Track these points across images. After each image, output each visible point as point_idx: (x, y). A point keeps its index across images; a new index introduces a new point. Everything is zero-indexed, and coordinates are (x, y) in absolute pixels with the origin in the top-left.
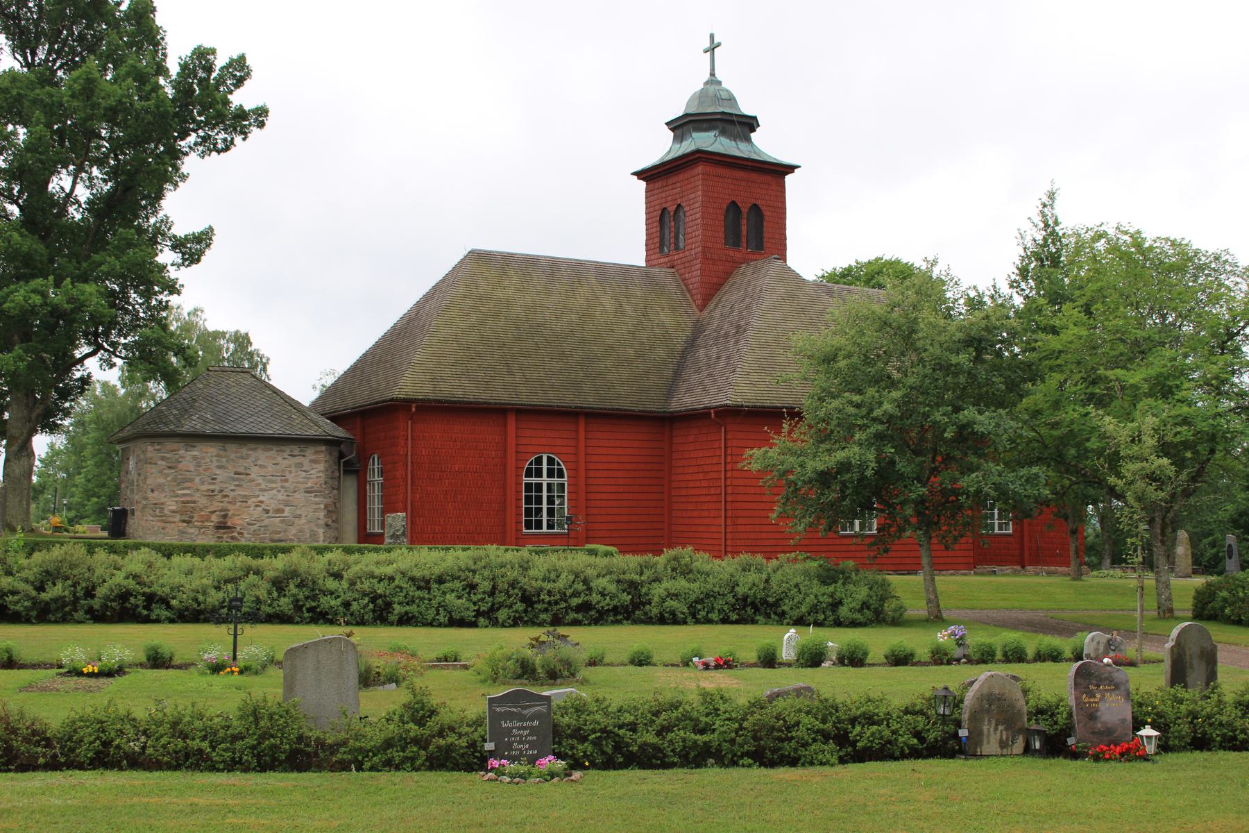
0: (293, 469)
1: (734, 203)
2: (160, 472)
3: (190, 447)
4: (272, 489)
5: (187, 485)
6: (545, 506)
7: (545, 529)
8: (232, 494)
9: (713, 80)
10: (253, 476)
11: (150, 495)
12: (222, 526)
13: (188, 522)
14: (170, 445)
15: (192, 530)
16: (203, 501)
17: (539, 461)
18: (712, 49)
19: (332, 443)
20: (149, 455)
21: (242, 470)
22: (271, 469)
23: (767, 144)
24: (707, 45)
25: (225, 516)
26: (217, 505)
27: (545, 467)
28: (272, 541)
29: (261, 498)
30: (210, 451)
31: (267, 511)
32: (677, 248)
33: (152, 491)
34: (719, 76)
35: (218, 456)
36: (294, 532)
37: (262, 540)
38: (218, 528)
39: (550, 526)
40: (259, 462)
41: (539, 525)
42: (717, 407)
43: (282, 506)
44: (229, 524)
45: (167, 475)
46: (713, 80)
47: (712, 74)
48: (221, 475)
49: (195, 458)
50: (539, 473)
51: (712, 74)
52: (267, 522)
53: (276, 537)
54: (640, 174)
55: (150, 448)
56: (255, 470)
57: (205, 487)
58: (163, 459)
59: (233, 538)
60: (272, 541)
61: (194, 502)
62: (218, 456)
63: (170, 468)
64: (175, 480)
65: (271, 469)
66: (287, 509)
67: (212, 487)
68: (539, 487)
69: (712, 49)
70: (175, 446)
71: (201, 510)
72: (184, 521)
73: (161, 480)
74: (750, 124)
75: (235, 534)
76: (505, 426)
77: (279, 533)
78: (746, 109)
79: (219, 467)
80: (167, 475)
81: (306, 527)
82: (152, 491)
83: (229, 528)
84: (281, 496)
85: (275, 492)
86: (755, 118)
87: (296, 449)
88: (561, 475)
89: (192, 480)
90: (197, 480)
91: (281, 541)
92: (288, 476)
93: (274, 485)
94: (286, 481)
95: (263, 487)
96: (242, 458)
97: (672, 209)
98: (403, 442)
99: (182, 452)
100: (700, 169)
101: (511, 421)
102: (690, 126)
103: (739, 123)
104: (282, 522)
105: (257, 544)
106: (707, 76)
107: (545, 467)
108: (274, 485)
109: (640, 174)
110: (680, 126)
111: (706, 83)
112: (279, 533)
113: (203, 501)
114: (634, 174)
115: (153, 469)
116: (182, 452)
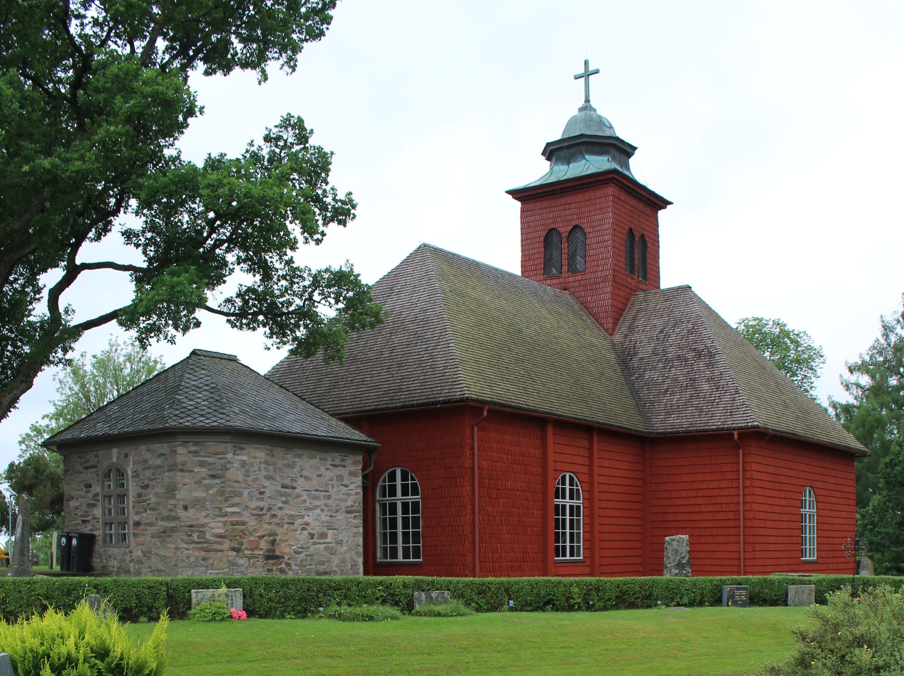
0: (335, 483)
1: (631, 229)
2: (199, 483)
3: (238, 449)
4: (316, 507)
5: (236, 500)
6: (400, 530)
7: (400, 558)
8: (280, 514)
9: (587, 107)
10: (299, 490)
11: (181, 513)
12: (271, 556)
13: (237, 550)
14: (212, 445)
15: (242, 561)
16: (252, 523)
17: (392, 477)
18: (587, 75)
19: (367, 451)
20: (179, 459)
21: (288, 482)
22: (315, 482)
23: (640, 170)
24: (582, 71)
25: (273, 542)
26: (265, 528)
27: (399, 482)
28: (318, 573)
29: (306, 519)
30: (256, 454)
31: (312, 536)
32: (573, 270)
33: (186, 508)
34: (593, 103)
35: (266, 462)
36: (336, 562)
37: (308, 572)
38: (268, 557)
39: (406, 556)
40: (305, 473)
41: (394, 554)
42: (742, 428)
43: (325, 530)
44: (277, 553)
45: (208, 487)
46: (587, 107)
47: (587, 100)
48: (271, 488)
49: (243, 464)
50: (393, 493)
51: (587, 100)
52: (312, 549)
53: (322, 568)
54: (516, 194)
55: (181, 450)
56: (301, 481)
57: (254, 504)
58: (202, 464)
59: (282, 571)
60: (318, 573)
61: (243, 524)
62: (266, 462)
63: (213, 477)
64: (221, 492)
65: (315, 482)
66: (330, 532)
67: (261, 504)
68: (405, 493)
69: (587, 75)
70: (221, 447)
71: (251, 534)
72: (233, 549)
73: (200, 494)
74: (625, 150)
75: (283, 566)
76: (544, 439)
77: (323, 563)
78: (623, 133)
79: (268, 478)
80: (208, 487)
81: (348, 556)
82: (186, 508)
83: (277, 557)
84: (325, 518)
85: (318, 511)
86: (635, 149)
87: (337, 458)
88: (415, 492)
89: (240, 495)
90: (246, 493)
91: (325, 573)
92: (332, 492)
93: (317, 503)
94: (329, 497)
95: (308, 504)
96: (288, 466)
97: (564, 230)
98: (468, 452)
99: (230, 456)
100: (611, 190)
101: (550, 430)
102: (583, 148)
103: (568, 147)
104: (326, 549)
105: (303, 576)
106: (581, 103)
107: (399, 482)
108: (317, 503)
109: (516, 194)
110: (552, 152)
111: (581, 110)
112: (323, 563)
113: (252, 523)
114: (509, 192)
115: (187, 478)
116: (230, 456)
